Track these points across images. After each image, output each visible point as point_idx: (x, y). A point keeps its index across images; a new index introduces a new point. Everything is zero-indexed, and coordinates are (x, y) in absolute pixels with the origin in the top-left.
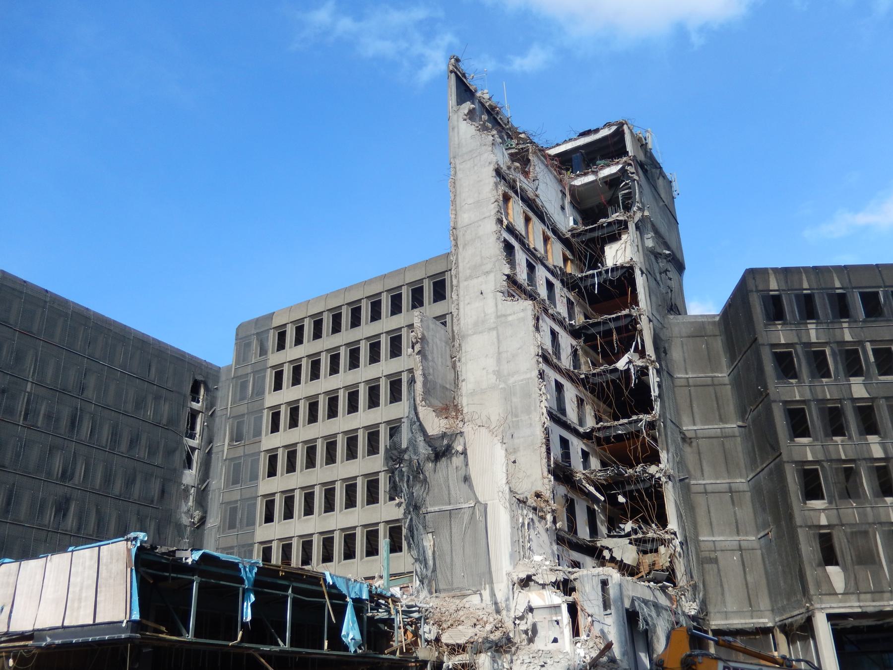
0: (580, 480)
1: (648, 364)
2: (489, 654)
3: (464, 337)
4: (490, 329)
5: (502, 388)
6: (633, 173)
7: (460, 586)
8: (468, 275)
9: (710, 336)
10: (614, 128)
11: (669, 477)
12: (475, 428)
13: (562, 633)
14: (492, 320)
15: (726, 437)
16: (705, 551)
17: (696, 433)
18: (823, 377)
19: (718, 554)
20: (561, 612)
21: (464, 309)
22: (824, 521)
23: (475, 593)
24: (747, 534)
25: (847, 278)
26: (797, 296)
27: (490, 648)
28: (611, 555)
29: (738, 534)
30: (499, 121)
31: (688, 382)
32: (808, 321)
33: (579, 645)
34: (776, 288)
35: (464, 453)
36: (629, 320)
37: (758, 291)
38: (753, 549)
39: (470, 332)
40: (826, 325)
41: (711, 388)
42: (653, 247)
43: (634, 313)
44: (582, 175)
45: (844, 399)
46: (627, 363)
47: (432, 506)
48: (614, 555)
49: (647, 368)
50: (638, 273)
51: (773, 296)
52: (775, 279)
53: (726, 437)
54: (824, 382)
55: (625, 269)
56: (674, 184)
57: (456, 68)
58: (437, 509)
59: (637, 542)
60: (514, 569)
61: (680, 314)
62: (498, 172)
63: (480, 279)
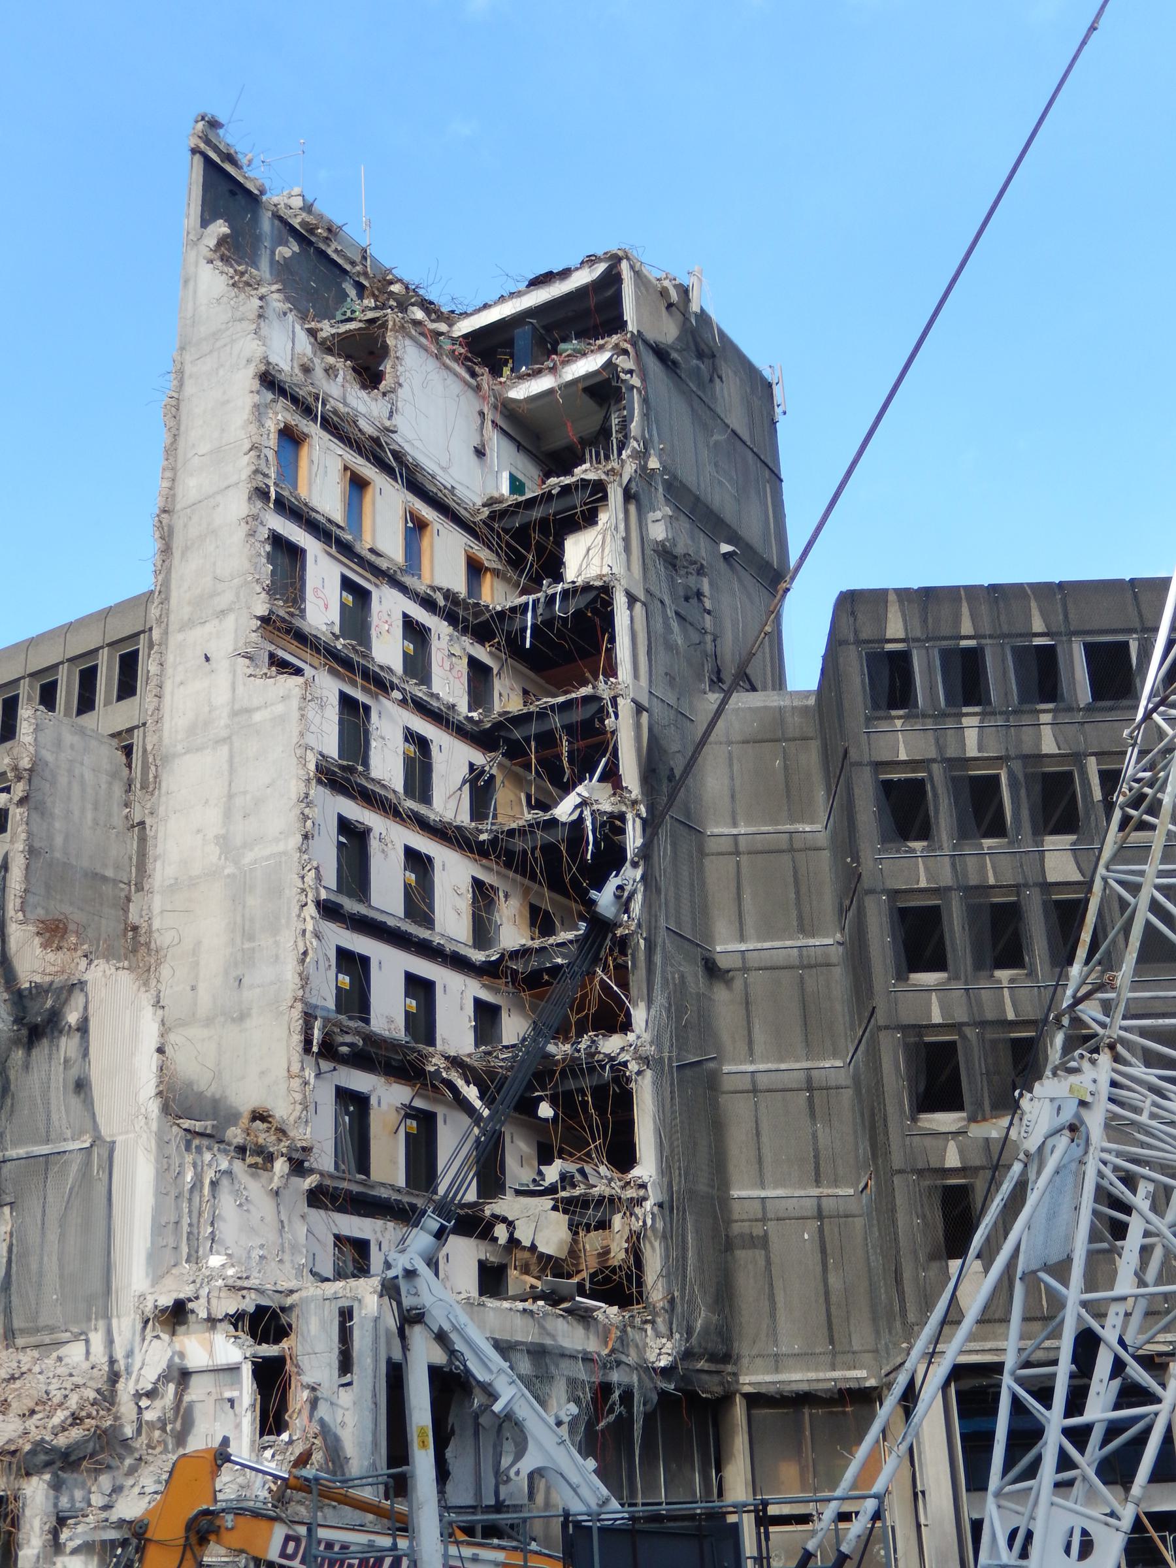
0: (438, 1072)
1: (624, 809)
2: (47, 1477)
3: (166, 759)
4: (217, 742)
5: (229, 876)
6: (631, 372)
7: (50, 1323)
8: (186, 617)
9: (795, 739)
10: (601, 268)
11: (645, 1060)
12: (108, 973)
13: (238, 1426)
14: (223, 719)
15: (810, 966)
16: (743, 1221)
17: (744, 959)
18: (987, 835)
19: (771, 1226)
20: (239, 1382)
21: (172, 694)
22: (952, 1160)
23: (76, 1338)
24: (836, 1183)
25: (1060, 610)
26: (946, 654)
27: (48, 1464)
28: (511, 1235)
29: (818, 1182)
30: (335, 256)
31: (736, 844)
32: (965, 710)
33: (268, 1453)
34: (901, 635)
35: (83, 1028)
36: (592, 708)
37: (859, 642)
38: (847, 1216)
39: (179, 748)
40: (1004, 717)
41: (786, 858)
42: (667, 539)
43: (603, 690)
44: (529, 375)
45: (1026, 885)
46: (576, 807)
47: (15, 1145)
48: (516, 1235)
49: (622, 817)
50: (620, 601)
51: (891, 654)
52: (899, 614)
53: (810, 966)
54: (985, 846)
55: (593, 594)
56: (777, 390)
57: (208, 142)
58: (21, 1152)
59: (567, 1206)
60: (153, 1286)
61: (754, 689)
62: (269, 380)
63: (208, 628)
